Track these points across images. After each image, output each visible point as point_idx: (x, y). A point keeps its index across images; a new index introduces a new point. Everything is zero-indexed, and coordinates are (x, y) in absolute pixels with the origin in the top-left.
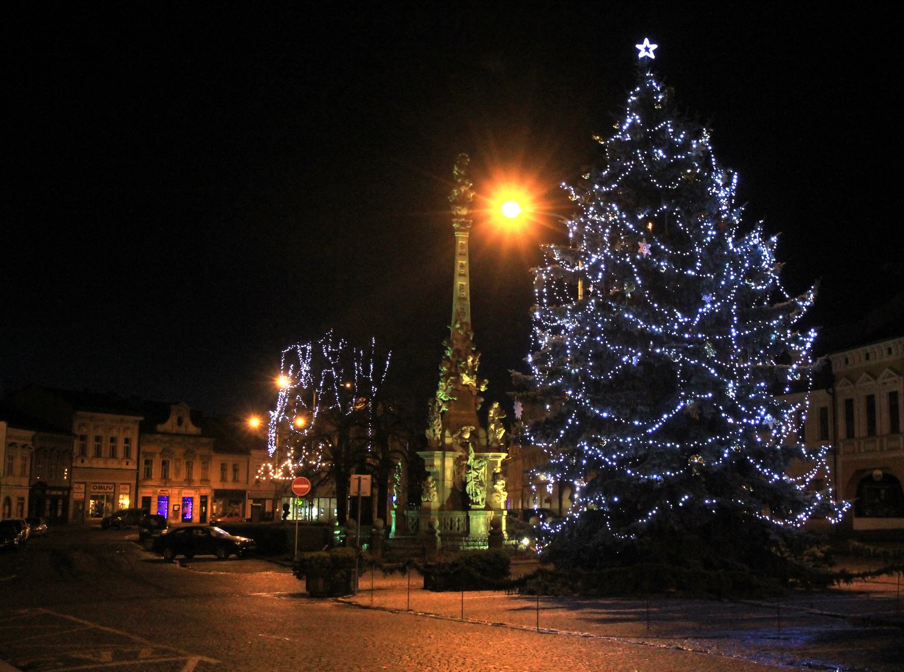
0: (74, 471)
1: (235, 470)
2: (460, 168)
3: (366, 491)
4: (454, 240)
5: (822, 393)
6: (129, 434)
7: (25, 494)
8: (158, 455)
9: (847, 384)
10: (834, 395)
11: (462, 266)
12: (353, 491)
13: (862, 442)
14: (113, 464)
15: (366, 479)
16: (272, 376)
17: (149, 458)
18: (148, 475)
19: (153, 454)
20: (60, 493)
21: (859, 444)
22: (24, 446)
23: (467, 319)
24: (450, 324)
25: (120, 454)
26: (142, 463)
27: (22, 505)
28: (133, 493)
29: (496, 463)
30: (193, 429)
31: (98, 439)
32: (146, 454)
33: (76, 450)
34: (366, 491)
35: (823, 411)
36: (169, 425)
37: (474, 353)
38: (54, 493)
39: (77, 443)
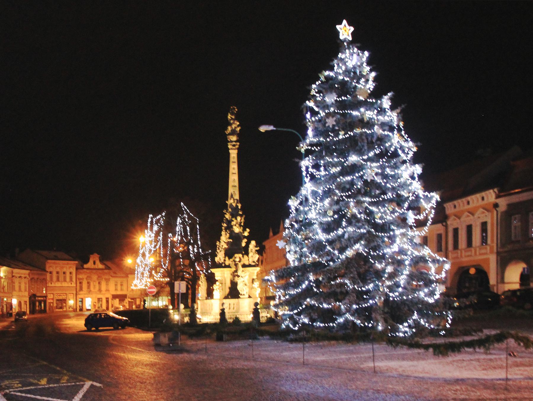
0: (48, 288)
1: (121, 285)
2: (232, 114)
3: (183, 290)
4: (229, 154)
5: (439, 226)
6: (71, 270)
7: (27, 299)
8: (85, 280)
9: (455, 220)
10: (446, 227)
11: (234, 169)
12: (176, 291)
13: (478, 249)
14: (65, 284)
15: (183, 284)
16: (135, 235)
17: (81, 281)
18: (81, 289)
19: (82, 279)
20: (42, 299)
21: (461, 252)
22: (25, 278)
23: (237, 197)
24: (228, 200)
25: (68, 279)
26: (78, 284)
27: (26, 304)
28: (75, 297)
29: (253, 273)
30: (101, 266)
31: (58, 273)
32: (80, 279)
33: (48, 278)
34: (183, 290)
35: (439, 236)
36: (90, 265)
37: (241, 216)
38: (39, 299)
39: (48, 275)
